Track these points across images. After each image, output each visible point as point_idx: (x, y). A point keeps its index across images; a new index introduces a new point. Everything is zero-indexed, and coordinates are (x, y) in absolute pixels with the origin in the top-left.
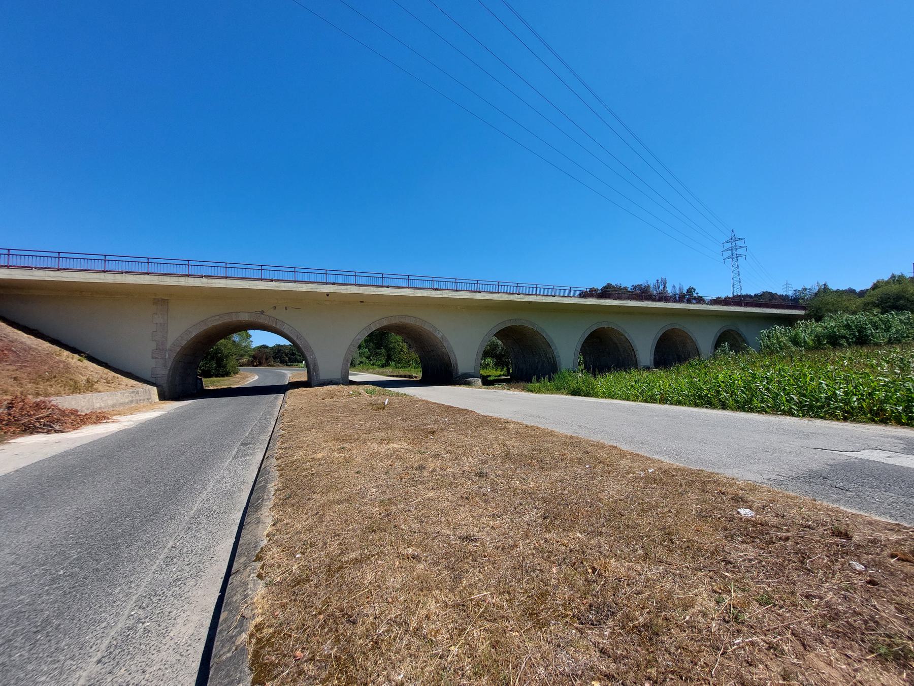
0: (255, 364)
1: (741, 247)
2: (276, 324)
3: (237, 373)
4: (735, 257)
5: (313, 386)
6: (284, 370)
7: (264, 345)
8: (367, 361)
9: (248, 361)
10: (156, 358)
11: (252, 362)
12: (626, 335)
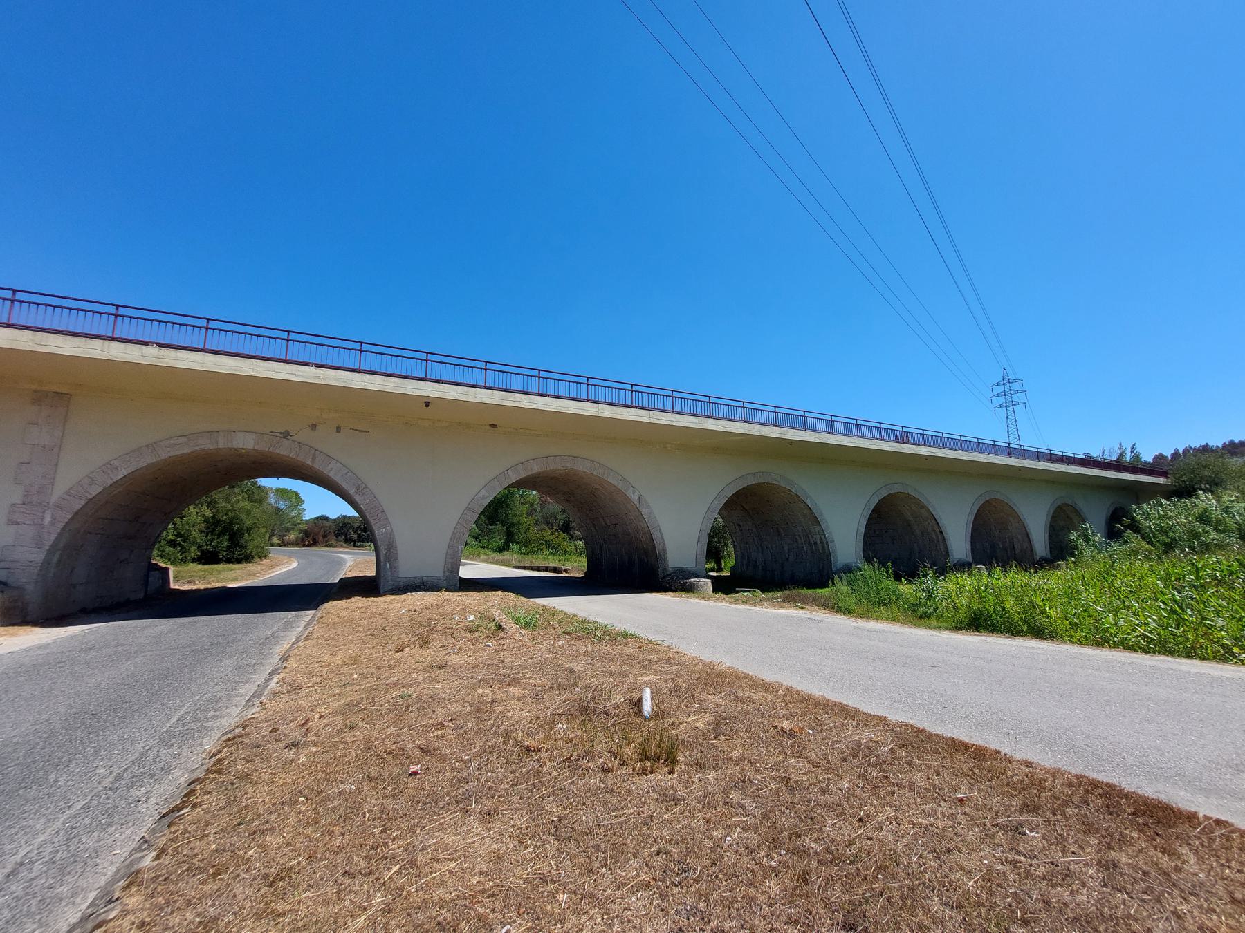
0: (307, 543)
1: (1017, 392)
2: (314, 459)
3: (265, 557)
4: (1010, 405)
5: (382, 591)
6: (345, 553)
7: (322, 516)
8: (474, 542)
9: (297, 538)
10: (18, 523)
11: (303, 540)
12: (929, 507)
